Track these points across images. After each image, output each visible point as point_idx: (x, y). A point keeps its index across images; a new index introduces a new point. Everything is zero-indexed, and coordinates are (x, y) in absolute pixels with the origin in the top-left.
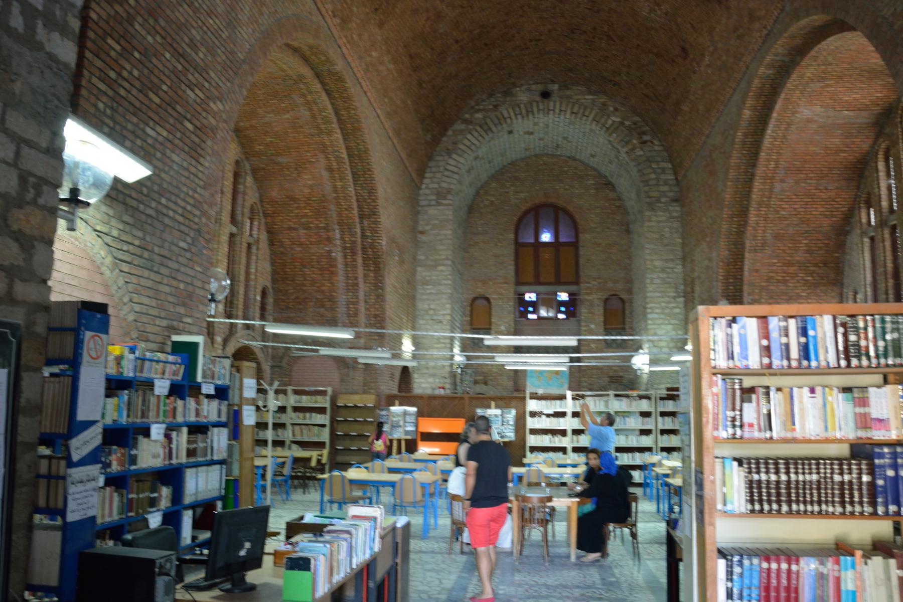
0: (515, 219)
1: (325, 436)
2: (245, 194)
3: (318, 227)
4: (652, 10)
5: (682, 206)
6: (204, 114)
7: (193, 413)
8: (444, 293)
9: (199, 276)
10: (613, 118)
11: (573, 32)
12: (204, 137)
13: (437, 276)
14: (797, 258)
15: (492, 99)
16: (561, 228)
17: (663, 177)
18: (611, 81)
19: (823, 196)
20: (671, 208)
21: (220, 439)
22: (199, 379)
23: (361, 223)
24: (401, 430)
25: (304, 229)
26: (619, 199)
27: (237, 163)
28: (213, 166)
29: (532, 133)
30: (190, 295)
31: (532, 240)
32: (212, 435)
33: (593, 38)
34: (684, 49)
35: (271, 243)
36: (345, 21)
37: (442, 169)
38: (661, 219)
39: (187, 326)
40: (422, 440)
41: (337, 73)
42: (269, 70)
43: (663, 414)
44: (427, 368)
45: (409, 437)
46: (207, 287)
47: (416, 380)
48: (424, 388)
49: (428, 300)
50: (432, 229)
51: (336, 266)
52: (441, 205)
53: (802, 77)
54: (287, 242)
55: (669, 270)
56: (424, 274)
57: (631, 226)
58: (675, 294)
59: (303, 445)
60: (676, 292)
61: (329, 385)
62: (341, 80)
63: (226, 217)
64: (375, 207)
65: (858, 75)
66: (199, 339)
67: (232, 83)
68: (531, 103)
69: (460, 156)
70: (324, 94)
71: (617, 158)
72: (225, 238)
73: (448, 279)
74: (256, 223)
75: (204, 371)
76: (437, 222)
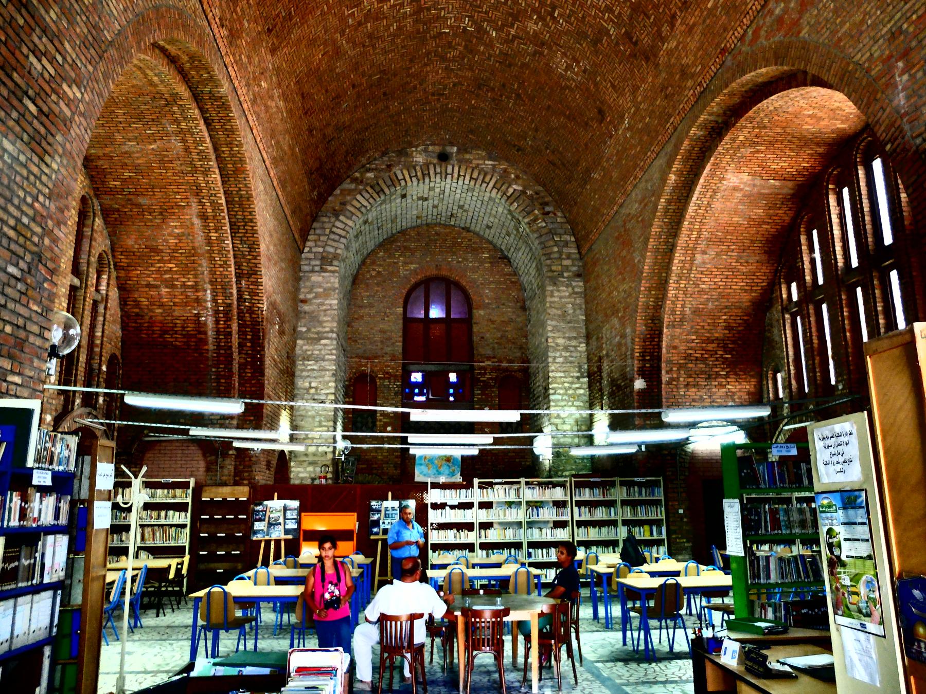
0: (404, 292)
1: (184, 539)
2: (92, 239)
3: (184, 285)
4: (569, 67)
5: (586, 282)
6: (54, 97)
7: (16, 514)
8: (328, 370)
9: (35, 318)
10: (514, 186)
11: (479, 88)
12: (53, 129)
13: (320, 350)
14: (717, 335)
15: (386, 159)
16: (453, 304)
17: (565, 250)
18: (515, 146)
19: (744, 269)
20: (574, 284)
21: (55, 552)
22: (30, 463)
23: (238, 282)
24: (281, 528)
25: (166, 287)
26: (515, 274)
27: (84, 200)
28: (63, 170)
29: (426, 199)
30: (21, 344)
31: (423, 316)
32: (44, 546)
33: (501, 96)
34: (601, 112)
35: (123, 302)
36: (234, 36)
37: (327, 231)
38: (563, 294)
39: (13, 387)
40: (304, 540)
41: (221, 98)
42: (135, 82)
43: (580, 504)
44: (306, 455)
45: (290, 537)
46: (46, 334)
47: (293, 469)
48: (302, 479)
49: (308, 376)
50: (315, 298)
51: (205, 333)
52: (326, 271)
53: (734, 140)
54: (144, 302)
55: (572, 349)
56: (304, 348)
57: (527, 303)
58: (578, 374)
59: (156, 552)
60: (579, 371)
61: (191, 476)
62: (225, 107)
63: (65, 263)
64: (256, 265)
65: (789, 141)
66: (34, 405)
67: (95, 68)
68: (427, 165)
69: (348, 218)
70: (202, 122)
71: (517, 230)
72: (63, 291)
73: (332, 354)
74: (105, 277)
75: (38, 452)
76: (321, 290)
